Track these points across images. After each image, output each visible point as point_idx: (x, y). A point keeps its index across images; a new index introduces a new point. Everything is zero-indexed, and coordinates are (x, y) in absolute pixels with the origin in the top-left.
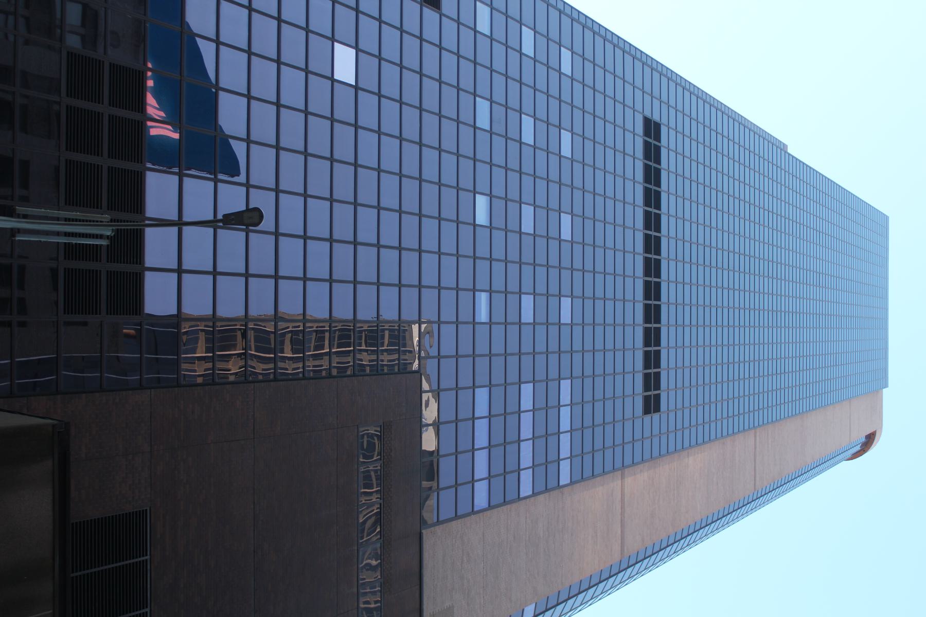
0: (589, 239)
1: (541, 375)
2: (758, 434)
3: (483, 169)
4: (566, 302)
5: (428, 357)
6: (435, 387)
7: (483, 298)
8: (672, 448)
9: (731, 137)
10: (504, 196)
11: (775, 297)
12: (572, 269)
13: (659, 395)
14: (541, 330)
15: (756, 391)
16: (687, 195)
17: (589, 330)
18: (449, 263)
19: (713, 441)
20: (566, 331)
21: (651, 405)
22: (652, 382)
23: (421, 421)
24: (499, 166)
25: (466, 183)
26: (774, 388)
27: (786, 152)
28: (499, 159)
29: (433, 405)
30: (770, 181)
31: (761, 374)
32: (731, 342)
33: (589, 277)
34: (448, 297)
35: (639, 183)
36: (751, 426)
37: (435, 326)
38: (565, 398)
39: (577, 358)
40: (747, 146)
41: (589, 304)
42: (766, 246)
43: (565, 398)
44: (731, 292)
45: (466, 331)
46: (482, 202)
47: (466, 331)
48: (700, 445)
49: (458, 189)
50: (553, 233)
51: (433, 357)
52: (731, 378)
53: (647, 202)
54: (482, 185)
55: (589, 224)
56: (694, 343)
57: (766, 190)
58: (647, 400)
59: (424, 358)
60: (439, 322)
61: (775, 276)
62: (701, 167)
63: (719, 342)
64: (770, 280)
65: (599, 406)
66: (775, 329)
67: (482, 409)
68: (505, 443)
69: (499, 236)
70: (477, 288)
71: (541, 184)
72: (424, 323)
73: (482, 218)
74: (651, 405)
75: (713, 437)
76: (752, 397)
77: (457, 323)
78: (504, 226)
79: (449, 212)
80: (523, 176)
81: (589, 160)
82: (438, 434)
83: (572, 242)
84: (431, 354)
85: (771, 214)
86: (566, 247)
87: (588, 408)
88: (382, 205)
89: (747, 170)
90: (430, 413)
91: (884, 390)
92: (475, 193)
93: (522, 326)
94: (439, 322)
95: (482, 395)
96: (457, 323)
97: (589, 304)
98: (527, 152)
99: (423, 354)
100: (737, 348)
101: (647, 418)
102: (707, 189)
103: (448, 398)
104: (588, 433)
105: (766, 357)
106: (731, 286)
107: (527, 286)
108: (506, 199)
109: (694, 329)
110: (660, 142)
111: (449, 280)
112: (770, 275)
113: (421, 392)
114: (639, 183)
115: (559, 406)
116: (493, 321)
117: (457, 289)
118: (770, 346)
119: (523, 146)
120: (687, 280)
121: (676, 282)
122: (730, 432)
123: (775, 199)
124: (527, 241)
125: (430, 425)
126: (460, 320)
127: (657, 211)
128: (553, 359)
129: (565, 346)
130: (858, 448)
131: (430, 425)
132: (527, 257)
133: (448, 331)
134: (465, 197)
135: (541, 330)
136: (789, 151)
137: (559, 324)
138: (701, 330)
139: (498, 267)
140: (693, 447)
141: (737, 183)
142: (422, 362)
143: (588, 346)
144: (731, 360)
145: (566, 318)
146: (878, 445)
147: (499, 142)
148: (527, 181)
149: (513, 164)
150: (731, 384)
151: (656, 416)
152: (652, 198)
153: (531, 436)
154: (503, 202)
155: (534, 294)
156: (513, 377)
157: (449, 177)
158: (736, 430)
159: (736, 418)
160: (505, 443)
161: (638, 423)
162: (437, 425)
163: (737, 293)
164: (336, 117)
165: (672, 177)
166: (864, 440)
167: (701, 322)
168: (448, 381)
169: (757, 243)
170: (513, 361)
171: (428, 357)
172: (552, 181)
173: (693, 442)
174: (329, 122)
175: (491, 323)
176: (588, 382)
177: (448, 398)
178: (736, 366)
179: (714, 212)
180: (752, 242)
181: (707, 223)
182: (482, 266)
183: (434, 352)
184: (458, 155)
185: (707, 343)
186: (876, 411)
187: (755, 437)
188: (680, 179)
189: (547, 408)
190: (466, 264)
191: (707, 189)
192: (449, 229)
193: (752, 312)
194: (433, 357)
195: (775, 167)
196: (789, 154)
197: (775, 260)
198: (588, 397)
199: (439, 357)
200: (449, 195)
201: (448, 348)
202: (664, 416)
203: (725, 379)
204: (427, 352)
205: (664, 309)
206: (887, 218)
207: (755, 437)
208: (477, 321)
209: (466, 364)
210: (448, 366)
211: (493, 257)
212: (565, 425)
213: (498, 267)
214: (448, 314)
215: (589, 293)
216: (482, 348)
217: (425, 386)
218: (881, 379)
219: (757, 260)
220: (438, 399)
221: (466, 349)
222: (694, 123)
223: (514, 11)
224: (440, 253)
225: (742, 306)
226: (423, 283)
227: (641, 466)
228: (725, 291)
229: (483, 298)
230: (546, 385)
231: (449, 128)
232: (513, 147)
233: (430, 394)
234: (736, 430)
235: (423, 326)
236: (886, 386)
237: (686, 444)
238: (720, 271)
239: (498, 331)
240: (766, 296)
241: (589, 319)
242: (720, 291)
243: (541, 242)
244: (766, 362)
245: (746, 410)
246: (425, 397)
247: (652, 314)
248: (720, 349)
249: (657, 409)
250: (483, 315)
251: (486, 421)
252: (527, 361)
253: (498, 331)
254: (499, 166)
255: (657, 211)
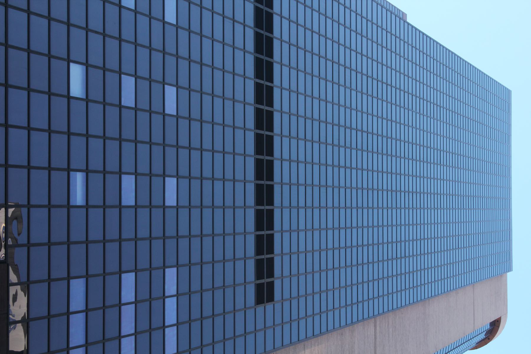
0: (195, 114)
1: (143, 263)
2: (378, 323)
3: (78, 35)
4: (171, 183)
5: (17, 245)
6: (24, 279)
7: (79, 179)
8: (287, 341)
9: (406, 40)
10: (102, 65)
11: (403, 177)
12: (213, 151)
13: (273, 282)
14: (144, 214)
15: (317, 289)
16: (354, 87)
17: (196, 213)
18: (40, 139)
19: (331, 331)
20: (171, 214)
21: (265, 294)
22: (265, 268)
23: (8, 318)
24: (96, 32)
25: (59, 49)
26: (419, 268)
27: (405, 21)
28: (143, 39)
29: (22, 300)
30: (389, 52)
31: (422, 252)
32: (399, 223)
33: (157, 151)
34: (39, 178)
35: (250, 53)
36: (371, 314)
37: (24, 211)
38: (171, 288)
39: (207, 241)
40: (418, 47)
41: (195, 184)
42: (354, 113)
43: (171, 288)
44: (309, 166)
45: (59, 215)
46: (77, 72)
47: (59, 215)
48: (317, 336)
49: (50, 56)
50: (112, 98)
51: (23, 245)
52: (349, 263)
53: (258, 74)
54: (78, 52)
55: (196, 97)
56: (448, 221)
57: (425, 82)
58: (259, 288)
59: (11, 246)
60: (29, 206)
61: (316, 138)
62: (329, 43)
63: (390, 223)
64: (370, 155)
65: (207, 296)
66: (439, 211)
67: (78, 302)
68: (151, 329)
69: (96, 110)
70: (72, 167)
71: (143, 53)
72: (11, 207)
73: (77, 89)
74: (265, 294)
75: (330, 327)
76: (449, 266)
77: (50, 206)
78: (102, 98)
79: (39, 82)
80: (123, 43)
81: (195, 27)
82: (27, 332)
83: (177, 117)
84: (20, 242)
85: (406, 94)
86: (129, 116)
87: (196, 298)
88: (32, 87)
89: (364, 40)
90: (19, 308)
91: (509, 274)
92: (69, 61)
93: (166, 210)
94: (29, 206)
95: (78, 287)
96: (50, 206)
97: (195, 184)
98: (170, 32)
99: (10, 242)
100: (403, 227)
101: (260, 309)
102: (422, 101)
103: (40, 291)
104: (196, 326)
105: (316, 247)
106: (398, 172)
107: (128, 166)
108: (104, 69)
109: (309, 211)
110: (272, 8)
111: (39, 158)
112: (370, 149)
113: (8, 284)
114: (250, 53)
115: (164, 297)
116: (90, 203)
117: (50, 169)
118: (415, 227)
119: (123, 10)
120: (316, 160)
121: (320, 164)
122: (349, 321)
123: (402, 76)
124: (129, 116)
125: (18, 322)
126: (192, 204)
127: (269, 84)
128: (196, 242)
129: (207, 230)
130: (483, 336)
131: (18, 322)
132: (171, 139)
133: (39, 216)
134: (58, 65)
135: (144, 214)
136: (409, 20)
137: (120, 207)
138: (316, 211)
139: (143, 149)
140: (310, 338)
141: (394, 72)
142: (9, 251)
143: (229, 229)
144: (323, 247)
145: (171, 200)
146: (503, 328)
147: (143, 21)
148: (171, 61)
149: (157, 43)
150: (349, 270)
151: (269, 306)
152: (264, 70)
153: (133, 331)
154: (151, 83)
155: (136, 174)
156: (157, 262)
157: (39, 43)
158: (355, 320)
159: (330, 314)
160: (151, 329)
161: (250, 313)
162: (26, 322)
163: (354, 171)
164: (90, 27)
165: (286, 117)
166: (488, 327)
167: (316, 204)
168: (39, 272)
169: (425, 133)
170: (157, 245)
171: (17, 245)
172: (156, 50)
173: (310, 334)
174: (26, 15)
175: (87, 206)
176: (196, 270)
177: (40, 291)
178: (385, 246)
179: (394, 107)
180: (429, 134)
181: (448, 136)
182: (78, 143)
183: (23, 239)
184: (50, 19)
185: (448, 221)
186: (500, 297)
187: (375, 326)
188: (309, 55)
189: (150, 300)
190: (60, 141)
191: (414, 97)
192: (39, 102)
193: (336, 190)
194: (23, 245)
195: (410, 47)
196: (408, 24)
197: (402, 138)
198: (196, 286)
199: (29, 245)
200: (39, 64)
201: (39, 234)
202: (278, 306)
203: (302, 270)
204: (15, 240)
205: (277, 189)
206: (508, 92)
207: (375, 326)
208: (72, 203)
209: (59, 252)
210: (39, 255)
211: (180, 144)
212: (171, 317)
213: (96, 144)
214: (39, 196)
215: (195, 172)
216: (77, 234)
217: (13, 278)
218: (505, 263)
219: (418, 147)
220: (27, 291)
221: (59, 235)
222: (369, 24)
223: (348, 4)
224: (29, 129)
225: (380, 187)
226: (10, 162)
227: (325, 336)
228: (316, 167)
229: (79, 179)
230: (150, 276)
231: (39, 102)
232: (157, 26)
233: (18, 287)
234: (355, 320)
235: (11, 211)
236: (510, 269)
237: (287, 341)
238: (422, 163)
239: (96, 215)
240: (425, 180)
241: (196, 201)
242: (422, 179)
243: (143, 117)
244: (433, 240)
245: (385, 293)
246: (12, 290)
247: (264, 195)
248: (429, 226)
249: (271, 298)
250: (78, 197)
251: (82, 316)
252: (78, 251)
253: (96, 215)
254: (96, 32)
255: (269, 84)
